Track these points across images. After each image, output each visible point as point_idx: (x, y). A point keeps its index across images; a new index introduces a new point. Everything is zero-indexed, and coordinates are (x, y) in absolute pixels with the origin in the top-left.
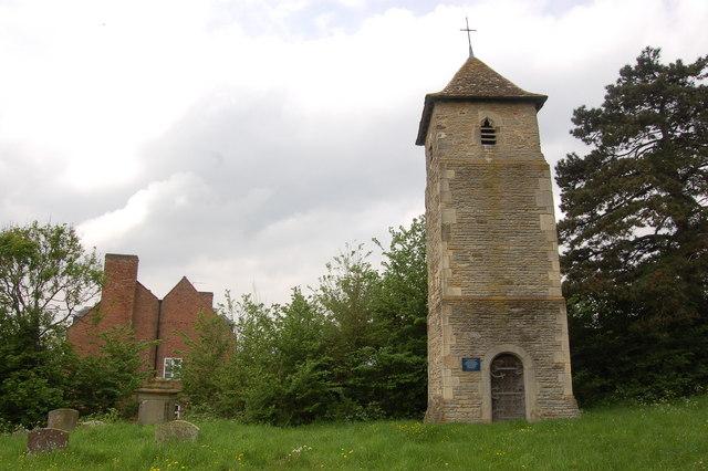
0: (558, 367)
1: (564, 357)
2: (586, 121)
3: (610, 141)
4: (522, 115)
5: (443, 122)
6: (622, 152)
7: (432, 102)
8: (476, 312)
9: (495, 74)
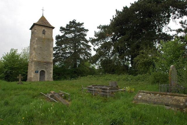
0: (51, 73)
1: (52, 71)
2: (62, 29)
3: (66, 33)
4: (50, 30)
5: (36, 29)
6: (67, 36)
7: (34, 24)
8: (39, 63)
9: (47, 21)
